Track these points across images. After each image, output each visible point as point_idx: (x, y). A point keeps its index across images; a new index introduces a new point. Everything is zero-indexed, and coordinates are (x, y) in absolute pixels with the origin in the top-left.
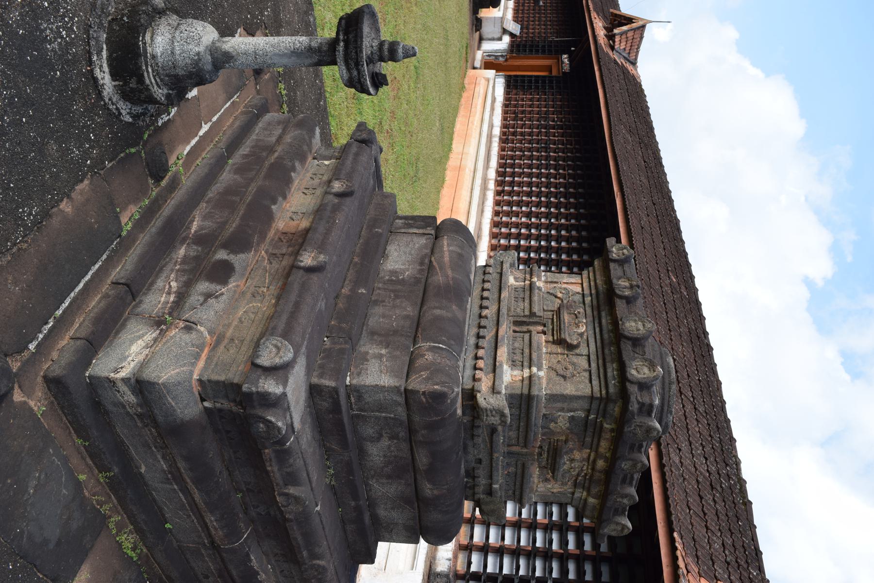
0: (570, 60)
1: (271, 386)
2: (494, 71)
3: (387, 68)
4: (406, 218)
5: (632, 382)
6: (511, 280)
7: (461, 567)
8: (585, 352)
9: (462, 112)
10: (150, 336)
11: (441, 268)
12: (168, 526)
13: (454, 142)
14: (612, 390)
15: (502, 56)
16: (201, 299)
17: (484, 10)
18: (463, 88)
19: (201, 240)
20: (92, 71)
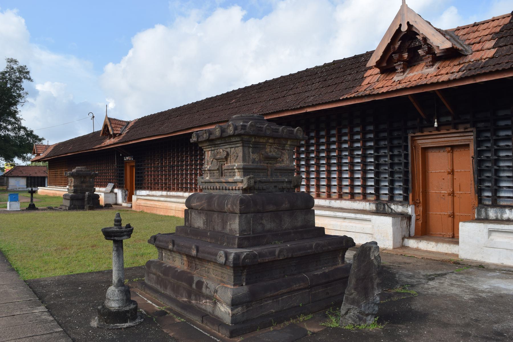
0: (127, 156)
1: (231, 257)
2: (133, 196)
3: (124, 225)
4: (185, 222)
5: (234, 133)
6: (207, 178)
7: (372, 198)
8: (229, 149)
9: (155, 212)
10: (219, 305)
11: (202, 205)
12: (301, 305)
13: (170, 215)
14: (239, 139)
15: (125, 192)
16: (208, 289)
17: (101, 203)
18: (142, 212)
19: (189, 297)
20: (124, 328)
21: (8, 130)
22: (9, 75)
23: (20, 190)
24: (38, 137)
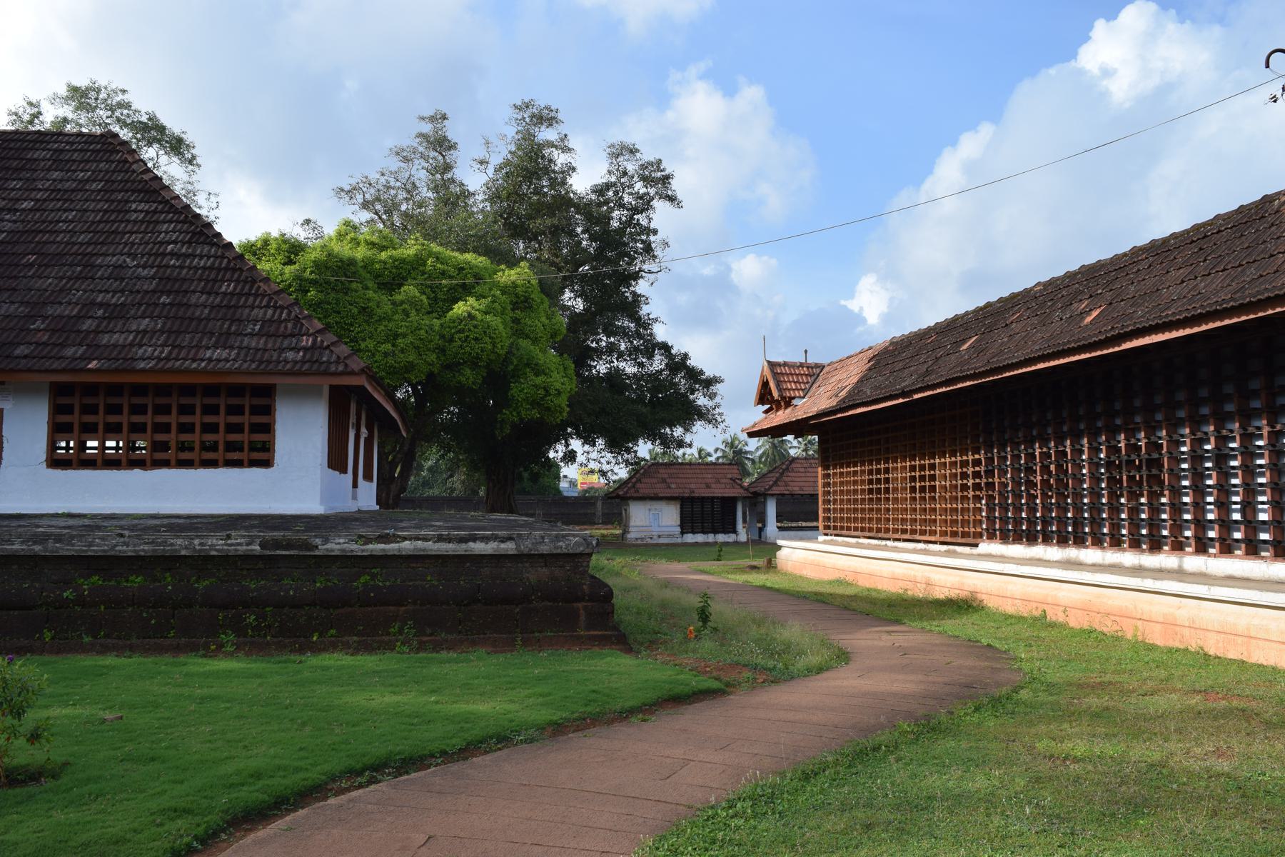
21: (620, 356)
22: (616, 193)
23: (662, 541)
24: (702, 372)
